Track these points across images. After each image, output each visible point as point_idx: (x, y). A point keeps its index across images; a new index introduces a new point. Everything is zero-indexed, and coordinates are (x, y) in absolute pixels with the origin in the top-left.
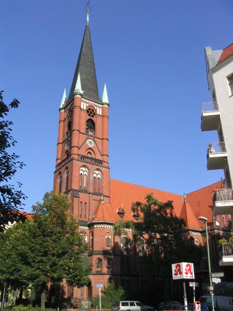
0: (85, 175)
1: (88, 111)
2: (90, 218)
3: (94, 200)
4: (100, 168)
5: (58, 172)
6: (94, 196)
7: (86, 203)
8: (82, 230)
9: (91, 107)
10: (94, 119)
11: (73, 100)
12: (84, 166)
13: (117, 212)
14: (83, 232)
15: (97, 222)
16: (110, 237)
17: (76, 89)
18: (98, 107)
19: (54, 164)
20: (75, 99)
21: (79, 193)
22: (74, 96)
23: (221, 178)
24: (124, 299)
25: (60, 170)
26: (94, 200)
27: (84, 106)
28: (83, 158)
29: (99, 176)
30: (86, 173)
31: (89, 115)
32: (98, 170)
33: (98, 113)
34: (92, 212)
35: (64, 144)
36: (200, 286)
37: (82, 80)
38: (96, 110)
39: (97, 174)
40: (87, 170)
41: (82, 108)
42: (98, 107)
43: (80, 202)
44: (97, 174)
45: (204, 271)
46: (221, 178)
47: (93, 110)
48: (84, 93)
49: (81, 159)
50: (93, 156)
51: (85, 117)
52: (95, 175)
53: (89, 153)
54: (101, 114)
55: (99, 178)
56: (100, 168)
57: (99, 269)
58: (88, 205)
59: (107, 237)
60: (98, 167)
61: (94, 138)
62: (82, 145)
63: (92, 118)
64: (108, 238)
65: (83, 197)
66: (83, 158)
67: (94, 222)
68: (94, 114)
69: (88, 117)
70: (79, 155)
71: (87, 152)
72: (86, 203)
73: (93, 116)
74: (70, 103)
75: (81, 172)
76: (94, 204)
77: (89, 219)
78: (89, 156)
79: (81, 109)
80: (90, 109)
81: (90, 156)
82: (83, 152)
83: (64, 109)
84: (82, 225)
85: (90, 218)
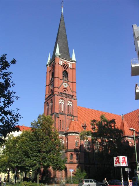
1: (63, 66)
5: (47, 102)
7: (63, 121)
10: (67, 70)
11: (55, 59)
12: (62, 99)
13: (82, 126)
16: (78, 141)
21: (59, 115)
27: (61, 63)
29: (71, 105)
30: (63, 103)
31: (64, 68)
33: (70, 67)
34: (67, 126)
39: (70, 104)
41: (60, 64)
43: (60, 120)
44: (70, 104)
49: (60, 94)
51: (62, 69)
52: (68, 104)
53: (65, 91)
55: (71, 106)
57: (72, 160)
59: (76, 141)
60: (69, 99)
61: (68, 82)
63: (66, 70)
65: (62, 117)
68: (67, 67)
69: (64, 70)
71: (63, 90)
73: (66, 69)
75: (60, 102)
78: (65, 92)
80: (64, 65)
82: (61, 90)
85: (66, 130)
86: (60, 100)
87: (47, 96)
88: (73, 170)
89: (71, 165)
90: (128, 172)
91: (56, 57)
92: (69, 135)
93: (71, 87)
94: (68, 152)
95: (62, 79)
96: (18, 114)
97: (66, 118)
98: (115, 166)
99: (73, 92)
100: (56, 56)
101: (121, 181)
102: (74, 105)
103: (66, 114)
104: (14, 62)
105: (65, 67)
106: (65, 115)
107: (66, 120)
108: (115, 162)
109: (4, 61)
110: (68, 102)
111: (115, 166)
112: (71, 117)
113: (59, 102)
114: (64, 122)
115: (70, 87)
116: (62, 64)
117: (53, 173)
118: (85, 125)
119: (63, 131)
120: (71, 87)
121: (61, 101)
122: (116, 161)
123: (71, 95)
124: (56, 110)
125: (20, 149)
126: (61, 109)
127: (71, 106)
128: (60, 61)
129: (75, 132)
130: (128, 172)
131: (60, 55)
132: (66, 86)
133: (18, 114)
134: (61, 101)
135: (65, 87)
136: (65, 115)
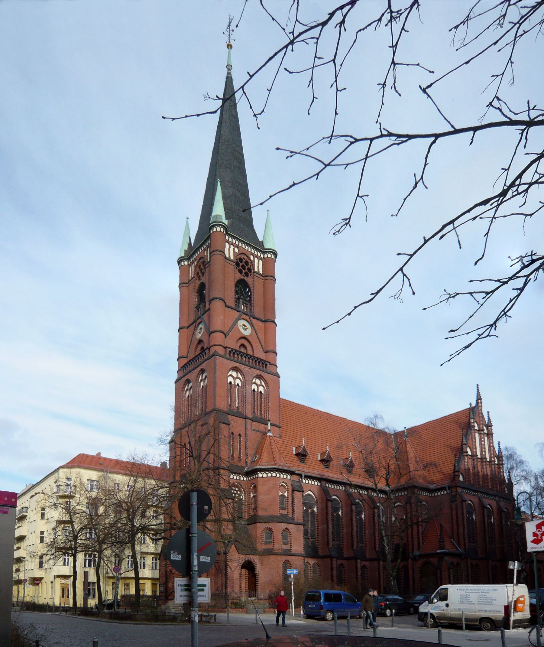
0: (238, 385)
1: (237, 264)
2: (249, 461)
3: (254, 430)
4: (264, 375)
5: (184, 379)
6: (254, 423)
7: (240, 435)
8: (235, 481)
9: (243, 256)
10: (249, 280)
11: (209, 237)
12: (235, 369)
13: (294, 453)
14: (238, 485)
15: (269, 467)
16: (286, 494)
17: (214, 214)
18: (257, 256)
19: (175, 366)
20: (212, 237)
21: (229, 417)
22: (211, 228)
23: (471, 404)
24: (296, 589)
25: (187, 377)
26: (254, 430)
27: (230, 252)
28: (234, 353)
29: (261, 389)
30: (238, 381)
31: (240, 272)
32: (259, 377)
33: (256, 270)
34: (251, 452)
35: (192, 327)
36: (286, 570)
37: (225, 198)
38: (253, 262)
39: (257, 386)
40: (240, 376)
41: (227, 256)
42: (257, 256)
43: (231, 432)
44: (257, 386)
45: (438, 551)
46: (471, 404)
47: (247, 263)
48: (231, 225)
49: (230, 355)
50: (250, 352)
51: (234, 275)
52: (254, 387)
53: (243, 345)
54: (261, 272)
55: (261, 392)
56: (264, 375)
57: (270, 546)
58: (243, 438)
59: (280, 494)
60: (258, 372)
61: (250, 316)
62: (230, 330)
63: (245, 278)
64: (283, 496)
65: (237, 425)
66: (234, 353)
67: (257, 467)
68: (249, 270)
69: (239, 276)
70: (226, 348)
71: (239, 344)
72: (240, 435)
73: (247, 275)
74: (200, 247)
75: (230, 379)
76: (253, 437)
77: (246, 462)
78: (243, 350)
79: (226, 258)
80: (241, 260)
81: (245, 352)
82: (232, 343)
83: (188, 259)
84: (235, 473)
85: (249, 461)
86: (230, 373)
87: (185, 361)
88: (295, 572)
89: (266, 559)
91: (215, 230)
92: (260, 475)
93: (261, 336)
94: (258, 524)
95: (233, 306)
96: (513, 63)
97: (249, 427)
98: (529, 550)
99: (266, 352)
100: (214, 226)
103: (250, 415)
106: (246, 418)
107: (249, 432)
108: (529, 537)
110: (254, 381)
111: (529, 550)
112: (262, 427)
113: (227, 377)
114: (243, 438)
115: (259, 336)
117: (95, 586)
118: (304, 449)
119: (239, 464)
120: (261, 336)
121: (231, 375)
122: (535, 534)
123: (262, 360)
124: (218, 400)
126: (236, 404)
127: (263, 392)
129: (280, 467)
131: (226, 222)
132: (247, 333)
133: (513, 63)
136: (246, 418)
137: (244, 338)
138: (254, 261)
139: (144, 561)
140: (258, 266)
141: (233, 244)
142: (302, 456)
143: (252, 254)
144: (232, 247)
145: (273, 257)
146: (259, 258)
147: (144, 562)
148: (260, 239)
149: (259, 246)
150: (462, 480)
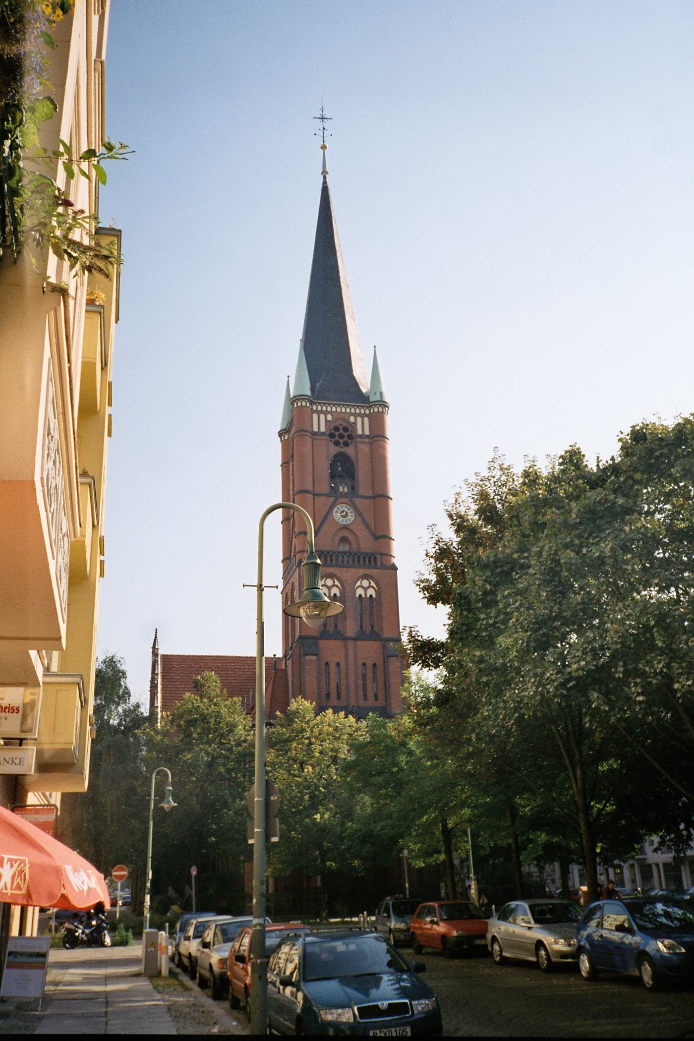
1: (332, 436)
10: (350, 451)
31: (337, 444)
53: (344, 540)
55: (371, 596)
60: (362, 572)
68: (350, 437)
69: (334, 450)
72: (338, 664)
86: (358, 584)
90: (118, 915)
101: (409, 893)
102: (387, 571)
104: (444, 625)
105: (341, 436)
106: (345, 639)
109: (656, 662)
116: (323, 429)
121: (361, 586)
125: (612, 560)
127: (374, 596)
128: (315, 416)
130: (118, 915)
134: (361, 586)
135: (342, 521)
137: (345, 527)
138: (355, 423)
139: (102, 558)
140: (362, 427)
141: (322, 412)
142: (6, 719)
143: (351, 414)
144: (322, 416)
145: (380, 410)
146: (363, 416)
147: (102, 562)
148: (365, 386)
149: (361, 399)
150: (442, 671)
